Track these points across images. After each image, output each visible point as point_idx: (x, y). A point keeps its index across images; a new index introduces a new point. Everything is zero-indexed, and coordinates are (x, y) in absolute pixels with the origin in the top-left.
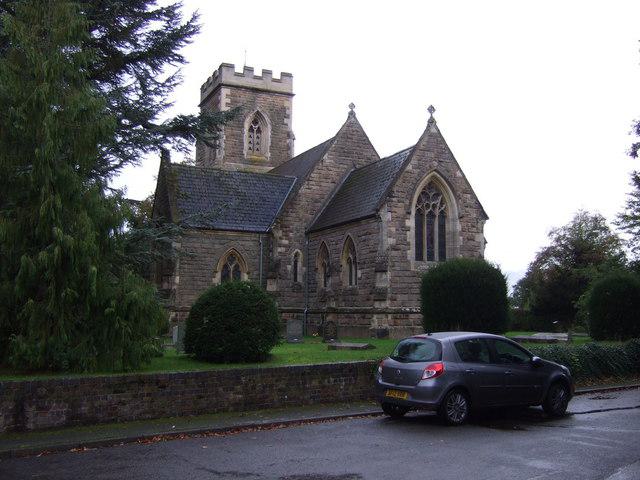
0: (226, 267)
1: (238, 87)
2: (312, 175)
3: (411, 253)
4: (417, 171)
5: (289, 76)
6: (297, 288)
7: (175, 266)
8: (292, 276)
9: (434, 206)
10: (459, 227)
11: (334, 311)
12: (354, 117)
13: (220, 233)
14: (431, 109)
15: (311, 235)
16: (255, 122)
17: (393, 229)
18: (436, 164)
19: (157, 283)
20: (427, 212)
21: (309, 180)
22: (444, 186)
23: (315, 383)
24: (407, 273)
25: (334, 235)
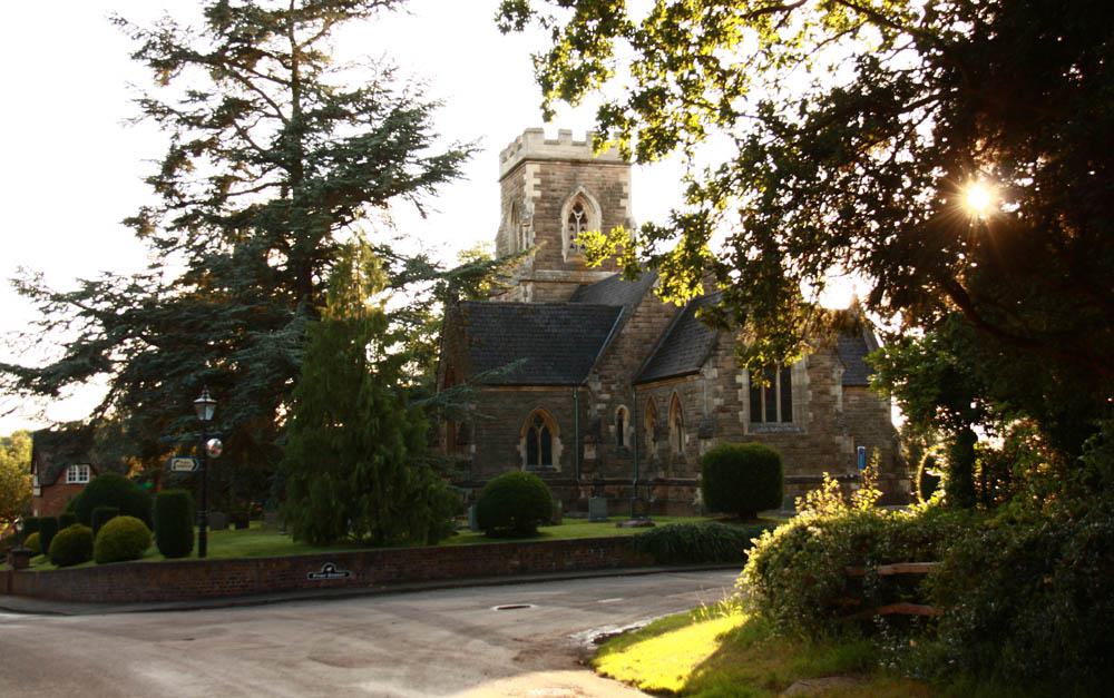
0: (532, 430)
1: (549, 160)
3: (744, 414)
8: (617, 439)
10: (807, 380)
16: (578, 208)
17: (720, 388)
21: (634, 316)
23: (577, 552)
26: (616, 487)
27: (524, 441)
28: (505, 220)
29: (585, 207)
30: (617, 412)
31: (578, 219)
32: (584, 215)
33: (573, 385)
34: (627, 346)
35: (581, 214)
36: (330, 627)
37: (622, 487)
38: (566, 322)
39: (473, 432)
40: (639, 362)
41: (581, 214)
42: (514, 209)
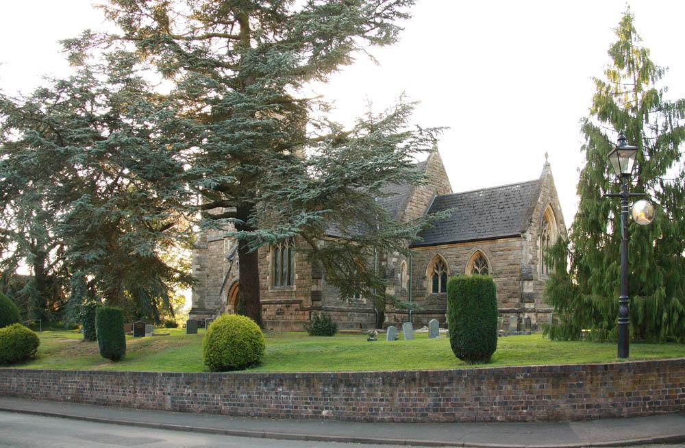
14: (546, 155)
17: (532, 247)
25: (454, 250)
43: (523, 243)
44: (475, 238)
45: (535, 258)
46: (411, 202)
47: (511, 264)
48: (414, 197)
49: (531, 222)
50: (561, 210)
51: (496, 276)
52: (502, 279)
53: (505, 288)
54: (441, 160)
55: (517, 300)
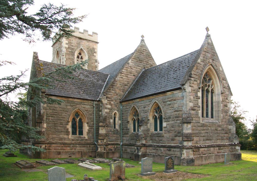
0: (74, 119)
2: (123, 70)
4: (202, 63)
5: (96, 34)
6: (116, 132)
7: (43, 117)
9: (209, 86)
11: (144, 145)
12: (144, 42)
13: (71, 100)
14: (207, 29)
15: (123, 103)
16: (80, 54)
17: (192, 97)
18: (211, 61)
19: (69, 35)
20: (206, 88)
22: (214, 75)
24: (199, 124)
25: (142, 102)
26: (113, 146)
27: (70, 124)
28: (54, 58)
29: (82, 54)
30: (113, 114)
31: (80, 58)
32: (82, 57)
33: (93, 101)
34: (118, 85)
35: (81, 56)
36: (19, 165)
37: (116, 146)
38: (87, 76)
39: (45, 117)
40: (122, 93)
41: (81, 56)
42: (58, 54)
43: (184, 93)
44: (154, 93)
45: (196, 105)
46: (121, 73)
47: (176, 111)
48: (123, 70)
49: (191, 77)
50: (223, 70)
51: (166, 120)
52: (171, 122)
53: (172, 129)
54: (147, 48)
55: (180, 139)
